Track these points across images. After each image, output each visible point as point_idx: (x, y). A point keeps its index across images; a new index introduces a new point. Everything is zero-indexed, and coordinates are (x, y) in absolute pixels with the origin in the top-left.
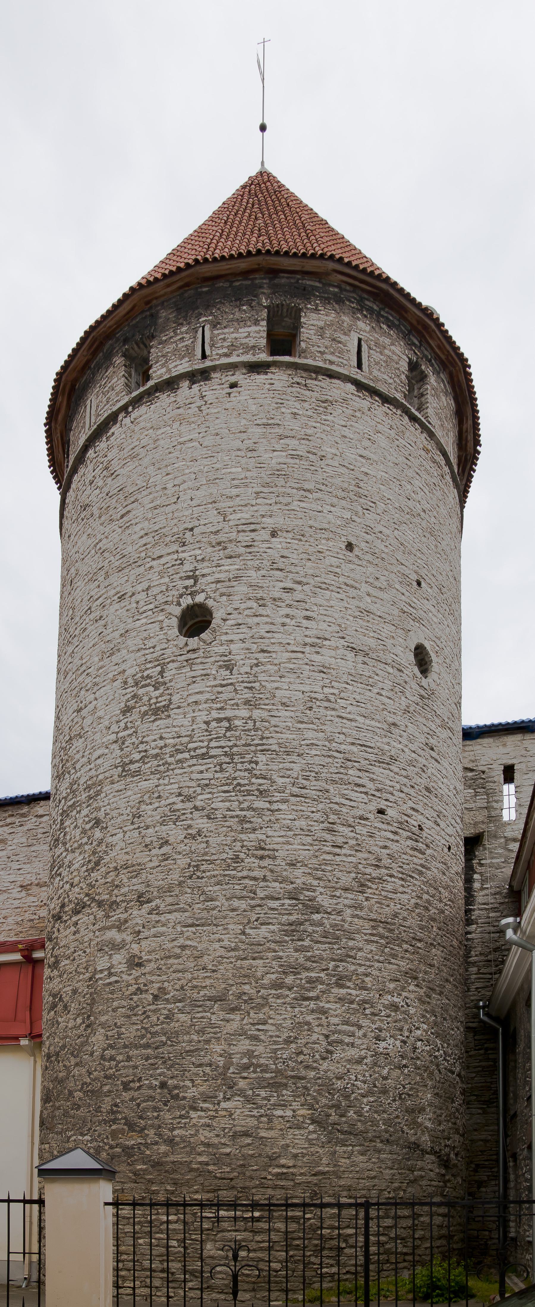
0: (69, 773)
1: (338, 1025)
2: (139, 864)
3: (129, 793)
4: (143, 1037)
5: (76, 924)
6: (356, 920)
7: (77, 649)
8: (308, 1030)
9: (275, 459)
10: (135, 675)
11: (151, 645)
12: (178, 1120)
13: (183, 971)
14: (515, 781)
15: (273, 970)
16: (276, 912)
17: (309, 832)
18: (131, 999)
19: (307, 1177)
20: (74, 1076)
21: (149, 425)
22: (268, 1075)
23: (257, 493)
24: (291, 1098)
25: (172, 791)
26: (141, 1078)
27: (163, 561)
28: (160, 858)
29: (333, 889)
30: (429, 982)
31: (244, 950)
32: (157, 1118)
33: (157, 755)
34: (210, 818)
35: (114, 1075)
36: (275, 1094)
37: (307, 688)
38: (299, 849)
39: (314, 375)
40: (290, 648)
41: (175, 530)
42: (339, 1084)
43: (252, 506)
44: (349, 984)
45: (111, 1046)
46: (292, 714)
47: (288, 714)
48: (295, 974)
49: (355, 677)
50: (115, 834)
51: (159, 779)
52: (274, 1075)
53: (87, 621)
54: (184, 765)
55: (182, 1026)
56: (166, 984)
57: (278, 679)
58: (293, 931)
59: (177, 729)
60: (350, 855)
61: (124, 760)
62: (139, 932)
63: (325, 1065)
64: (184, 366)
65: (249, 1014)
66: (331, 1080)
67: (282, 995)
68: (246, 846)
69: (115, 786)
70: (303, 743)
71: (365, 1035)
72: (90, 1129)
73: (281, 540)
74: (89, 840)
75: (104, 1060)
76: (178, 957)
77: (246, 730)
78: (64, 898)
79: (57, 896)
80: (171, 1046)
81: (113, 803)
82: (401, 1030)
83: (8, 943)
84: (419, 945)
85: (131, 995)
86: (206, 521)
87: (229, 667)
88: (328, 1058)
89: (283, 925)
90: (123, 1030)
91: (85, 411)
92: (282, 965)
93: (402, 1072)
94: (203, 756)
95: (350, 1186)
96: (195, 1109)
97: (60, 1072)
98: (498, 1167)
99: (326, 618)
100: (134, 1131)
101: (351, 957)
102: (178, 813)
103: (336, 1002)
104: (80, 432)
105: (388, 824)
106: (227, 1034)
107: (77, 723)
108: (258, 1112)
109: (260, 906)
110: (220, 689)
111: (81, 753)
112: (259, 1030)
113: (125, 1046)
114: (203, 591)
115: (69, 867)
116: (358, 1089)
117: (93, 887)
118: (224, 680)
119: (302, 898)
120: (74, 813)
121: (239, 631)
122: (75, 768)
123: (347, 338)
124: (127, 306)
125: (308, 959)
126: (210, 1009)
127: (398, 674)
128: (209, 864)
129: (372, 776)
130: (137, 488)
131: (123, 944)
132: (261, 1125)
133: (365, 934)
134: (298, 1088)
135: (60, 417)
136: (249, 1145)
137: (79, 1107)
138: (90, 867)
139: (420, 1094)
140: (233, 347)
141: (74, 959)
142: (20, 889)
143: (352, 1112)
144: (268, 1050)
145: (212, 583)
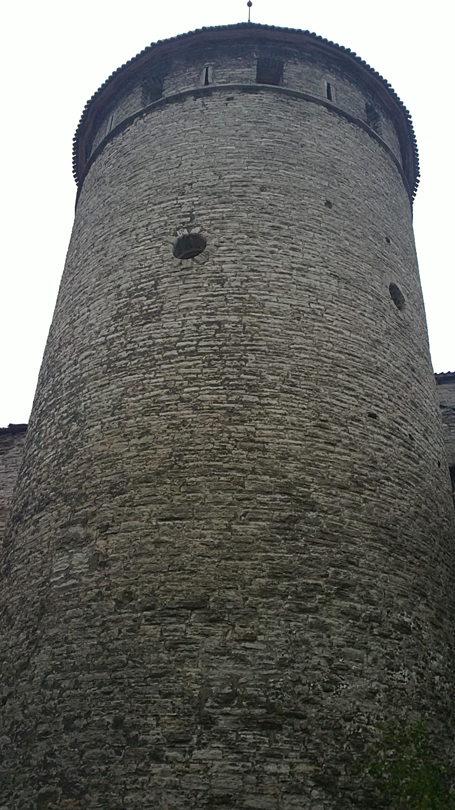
2: (116, 455)
4: (98, 655)
5: (37, 521)
6: (355, 522)
10: (129, 288)
11: (146, 265)
16: (266, 507)
17: (300, 427)
18: (89, 606)
22: (257, 711)
24: (287, 746)
26: (90, 712)
27: (163, 205)
28: (139, 448)
30: (438, 603)
31: (229, 548)
32: (104, 774)
33: (143, 354)
36: (267, 740)
37: (295, 302)
38: (291, 444)
40: (278, 270)
41: (177, 184)
44: (352, 596)
45: (56, 668)
46: (281, 322)
47: (276, 321)
48: (290, 579)
49: (339, 298)
50: (93, 426)
51: (144, 374)
54: (172, 361)
55: (149, 641)
56: (133, 588)
57: (268, 293)
58: (286, 529)
59: (167, 330)
63: (328, 700)
65: (234, 626)
68: (234, 437)
70: (291, 346)
71: (375, 661)
73: (269, 193)
74: (64, 434)
76: (150, 554)
77: (235, 333)
78: (29, 496)
80: (133, 668)
81: (94, 397)
84: (423, 558)
85: (89, 601)
87: (221, 282)
88: (332, 691)
89: (274, 522)
90: (74, 646)
91: (107, 124)
92: (274, 568)
93: (423, 715)
94: (192, 353)
99: (310, 251)
100: (70, 796)
102: (162, 405)
103: (339, 617)
105: (380, 428)
106: (206, 652)
107: (69, 332)
108: (243, 766)
109: (248, 499)
110: (211, 299)
111: (68, 357)
112: (246, 649)
113: (75, 669)
114: (199, 226)
116: (373, 736)
118: (215, 291)
119: (295, 494)
125: (304, 562)
127: (378, 302)
128: (193, 454)
129: (360, 382)
132: (248, 787)
133: (367, 539)
141: (29, 562)
144: (256, 676)
145: (207, 220)
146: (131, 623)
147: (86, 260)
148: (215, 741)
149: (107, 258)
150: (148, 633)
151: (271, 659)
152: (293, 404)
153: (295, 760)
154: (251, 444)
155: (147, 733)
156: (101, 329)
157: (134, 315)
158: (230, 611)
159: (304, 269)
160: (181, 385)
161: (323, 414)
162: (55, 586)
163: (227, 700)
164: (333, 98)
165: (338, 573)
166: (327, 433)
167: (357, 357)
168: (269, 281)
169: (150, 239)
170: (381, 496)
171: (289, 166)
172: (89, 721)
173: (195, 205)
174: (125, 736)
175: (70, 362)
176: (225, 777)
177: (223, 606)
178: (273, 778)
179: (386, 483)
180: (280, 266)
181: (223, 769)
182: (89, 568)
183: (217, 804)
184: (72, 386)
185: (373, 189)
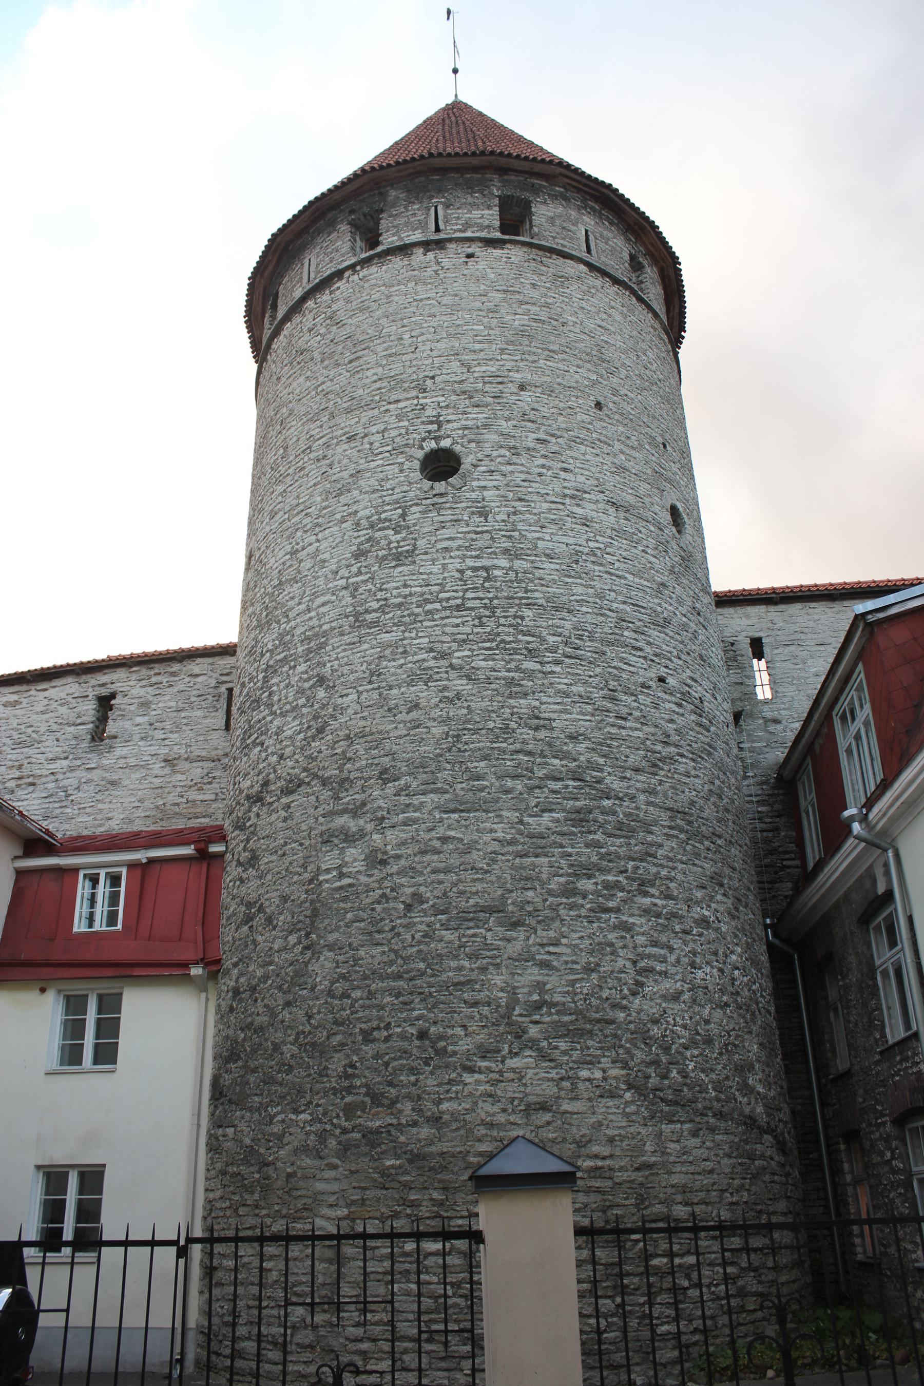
0: (278, 622)
1: (646, 947)
2: (380, 732)
3: (365, 646)
4: (391, 963)
5: (288, 806)
6: (652, 809)
7: (290, 489)
8: (612, 954)
9: (519, 321)
11: (389, 487)
12: (447, 1087)
13: (446, 871)
14: (765, 655)
15: (561, 872)
17: (587, 699)
19: (629, 1173)
20: (283, 1021)
22: (566, 1018)
24: (599, 1052)
25: (422, 646)
26: (389, 1023)
27: (401, 405)
31: (523, 844)
33: (399, 606)
34: (470, 679)
35: (348, 1019)
36: (578, 1047)
39: (548, 255)
40: (549, 498)
41: (415, 377)
42: (655, 1031)
43: (498, 360)
46: (558, 567)
47: (553, 566)
49: (619, 533)
50: (347, 695)
51: (404, 632)
52: (574, 1017)
53: (306, 459)
54: (435, 617)
56: (422, 889)
57: (539, 529)
58: (582, 820)
59: (425, 577)
60: (636, 729)
61: (358, 608)
62: (383, 818)
64: (417, 236)
66: (645, 1024)
67: (576, 906)
69: (346, 637)
71: (678, 961)
72: (310, 1102)
73: (530, 393)
74: (308, 701)
75: (333, 997)
79: (256, 771)
80: (432, 976)
81: (343, 658)
82: (715, 954)
83: (143, 835)
84: (719, 842)
85: (373, 903)
86: (449, 371)
87: (484, 514)
92: (572, 865)
93: (724, 1013)
94: (458, 608)
95: (684, 1186)
96: (471, 1070)
97: (258, 1015)
98: (819, 1150)
99: (583, 471)
101: (651, 855)
103: (641, 916)
104: (295, 286)
105: (671, 694)
107: (291, 566)
110: (474, 536)
111: (296, 600)
112: (549, 953)
113: (365, 977)
114: (449, 436)
115: (277, 734)
117: (314, 759)
118: (478, 527)
119: (588, 779)
120: (286, 669)
121: (491, 478)
123: (575, 228)
124: (356, 184)
125: (602, 857)
126: (485, 924)
127: (660, 533)
129: (648, 638)
130: (368, 337)
131: (362, 834)
132: (563, 1093)
134: (606, 1037)
135: (267, 274)
136: (549, 1123)
137: (290, 1069)
138: (309, 734)
139: (746, 1045)
140: (467, 226)
141: (284, 854)
142: (163, 764)
143: (675, 1071)
144: (563, 982)
145: (459, 429)
147: (303, 468)
148: (526, 1050)
150: (445, 939)
151: (577, 963)
152: (579, 672)
153: (608, 1066)
154: (536, 721)
155: (455, 1044)
156: (339, 568)
157: (380, 553)
158: (529, 914)
159: (578, 496)
160: (450, 648)
161: (611, 682)
163: (537, 1007)
164: (593, 252)
167: (644, 608)
168: (539, 514)
170: (676, 776)
171: (551, 354)
172: (391, 1032)
173: (441, 407)
174: (432, 1047)
175: (301, 607)
176: (540, 1085)
177: (522, 908)
178: (587, 1083)
179: (680, 760)
180: (551, 493)
181: (537, 1077)
182: (367, 866)
183: (534, 1110)
184: (309, 639)
185: (646, 378)
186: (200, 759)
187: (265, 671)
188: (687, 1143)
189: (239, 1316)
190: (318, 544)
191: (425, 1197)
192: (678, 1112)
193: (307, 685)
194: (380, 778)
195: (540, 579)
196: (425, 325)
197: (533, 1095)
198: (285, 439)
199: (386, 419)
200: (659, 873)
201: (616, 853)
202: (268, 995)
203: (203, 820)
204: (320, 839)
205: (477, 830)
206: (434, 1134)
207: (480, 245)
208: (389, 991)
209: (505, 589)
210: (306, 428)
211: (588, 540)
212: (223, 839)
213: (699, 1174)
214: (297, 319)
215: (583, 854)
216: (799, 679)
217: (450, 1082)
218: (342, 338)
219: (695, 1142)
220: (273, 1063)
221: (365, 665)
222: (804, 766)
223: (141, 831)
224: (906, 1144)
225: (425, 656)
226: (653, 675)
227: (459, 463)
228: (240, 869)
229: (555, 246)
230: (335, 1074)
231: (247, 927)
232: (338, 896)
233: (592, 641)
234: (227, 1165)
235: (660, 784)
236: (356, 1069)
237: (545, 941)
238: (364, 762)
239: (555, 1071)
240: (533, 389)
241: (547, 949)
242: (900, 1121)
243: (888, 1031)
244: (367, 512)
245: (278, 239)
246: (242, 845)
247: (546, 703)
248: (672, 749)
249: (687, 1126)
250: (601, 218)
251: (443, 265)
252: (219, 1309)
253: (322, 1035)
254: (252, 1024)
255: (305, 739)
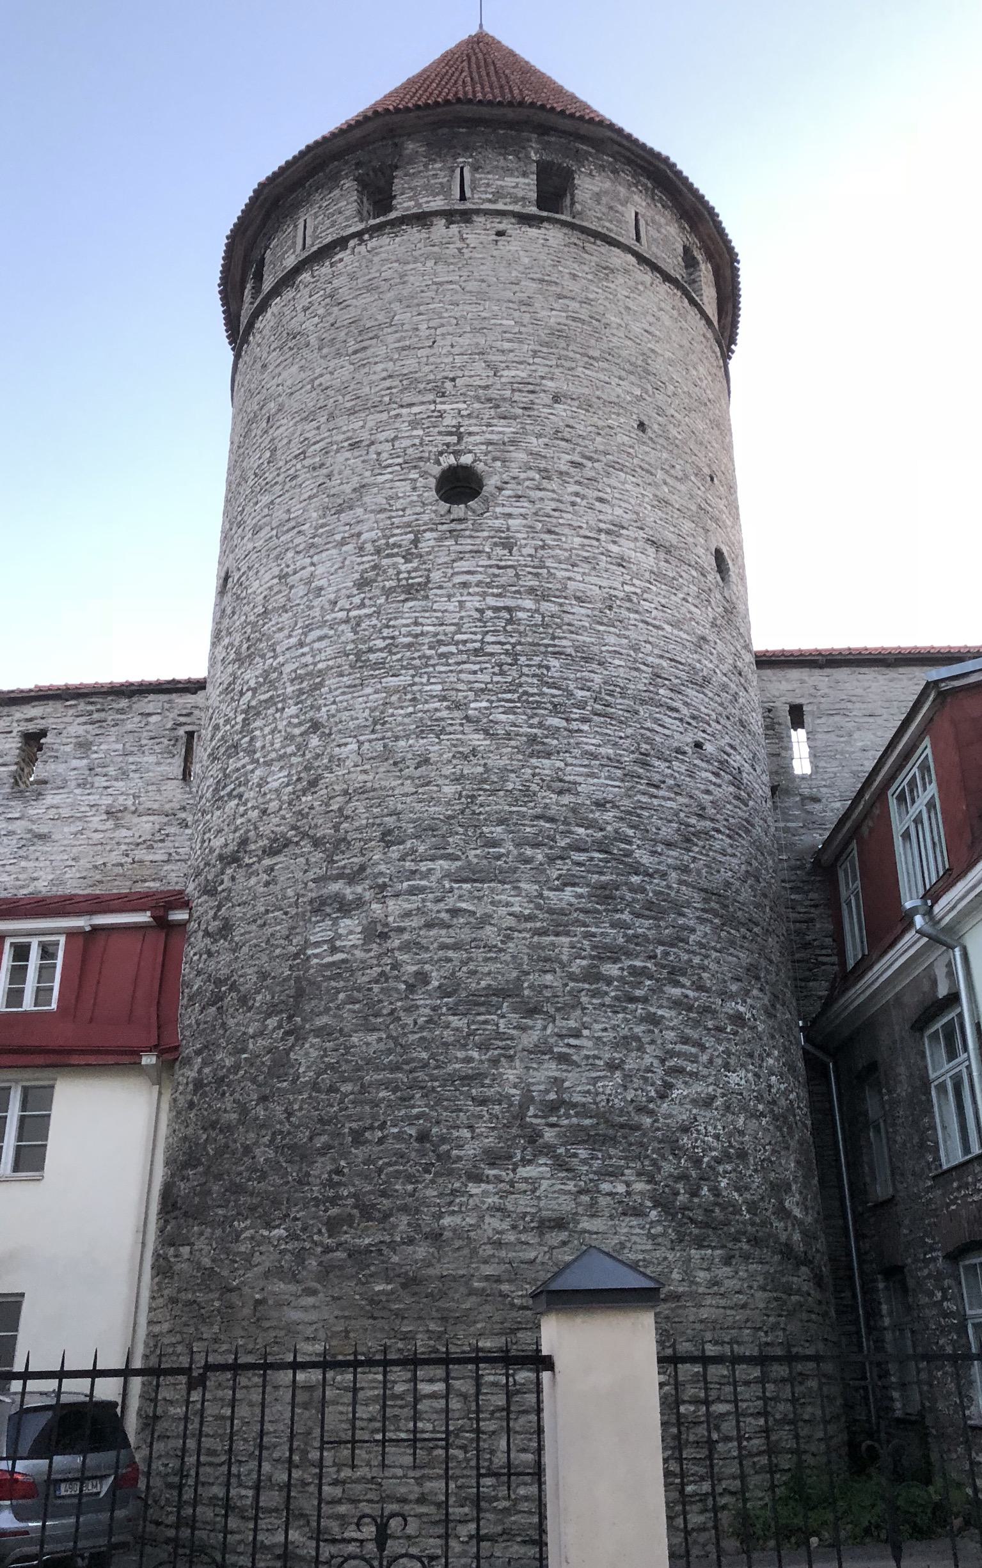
0: (263, 656)
3: (368, 690)
4: (389, 1052)
5: (271, 869)
6: (684, 888)
7: (279, 500)
8: (638, 1050)
9: (555, 318)
11: (399, 507)
12: (448, 1199)
13: (456, 947)
15: (584, 953)
21: (394, 258)
22: (587, 1122)
23: (535, 352)
26: (385, 1122)
27: (415, 410)
29: (653, 842)
31: (542, 920)
33: (409, 646)
37: (605, 583)
39: (592, 240)
40: (582, 532)
41: (432, 377)
46: (589, 612)
47: (583, 611)
49: (658, 576)
50: (346, 744)
51: (413, 676)
53: (299, 466)
54: (450, 661)
58: (607, 897)
59: (439, 614)
60: (669, 799)
64: (438, 203)
69: (345, 679)
71: (711, 1061)
73: (566, 407)
74: (298, 750)
75: (319, 1091)
79: (233, 827)
80: (436, 1067)
81: (341, 702)
84: (756, 930)
85: (369, 982)
86: (472, 373)
87: (508, 545)
94: (477, 653)
96: (478, 1178)
97: (225, 1111)
100: (370, 1219)
101: (682, 940)
103: (670, 1008)
104: (286, 252)
105: (708, 762)
110: (496, 571)
111: (286, 632)
112: (569, 1045)
114: (470, 452)
115: (260, 786)
118: (501, 560)
119: (615, 851)
120: (271, 711)
121: (518, 504)
122: (274, 650)
125: (629, 939)
127: (703, 579)
131: (359, 903)
132: (580, 1210)
134: (631, 1145)
137: (263, 1177)
138: (299, 787)
141: (265, 924)
142: (105, 817)
143: (706, 1188)
145: (482, 444)
146: (427, 1011)
147: (295, 477)
149: (333, 483)
150: (453, 1025)
151: (600, 1058)
152: (608, 731)
154: (561, 784)
155: (460, 1147)
159: (615, 531)
160: (465, 697)
161: (644, 746)
162: (315, 961)
165: (667, 954)
166: (648, 771)
169: (400, 464)
170: (711, 853)
174: (433, 1151)
177: (540, 992)
178: (609, 1198)
180: (585, 526)
183: (549, 1227)
184: (301, 679)
186: (150, 812)
187: (246, 712)
188: (717, 1272)
189: (187, 1476)
190: (313, 568)
191: (421, 1329)
192: (709, 1236)
193: (297, 731)
194: (382, 840)
195: (569, 624)
196: (445, 315)
197: (548, 1210)
198: (273, 439)
199: (397, 425)
200: (691, 961)
201: (645, 935)
202: (238, 1089)
203: (151, 884)
204: (309, 908)
205: (491, 903)
206: (433, 1254)
207: (513, 220)
208: (385, 1084)
209: (530, 633)
210: (300, 427)
211: (623, 583)
212: (186, 905)
213: (732, 1308)
214: (289, 294)
215: (608, 934)
216: (842, 753)
217: (454, 1192)
218: (345, 323)
219: (727, 1270)
220: (243, 1168)
221: (367, 711)
222: (849, 850)
223: (75, 895)
224: (960, 1283)
225: (437, 705)
226: (689, 740)
227: (481, 486)
228: (208, 941)
229: (600, 229)
230: (318, 1181)
231: (214, 1009)
232: (329, 973)
233: (624, 698)
234: (179, 1291)
235: (693, 862)
236: (344, 1175)
237: (564, 1032)
238: (364, 822)
239: (572, 1183)
240: (569, 401)
241: (566, 1041)
242: (955, 1256)
243: (942, 1153)
244: (372, 535)
245: (266, 191)
246: (211, 913)
247: (571, 765)
248: (708, 824)
249: (719, 1252)
250: (653, 199)
251: (468, 241)
252: (162, 1468)
253: (303, 1136)
254: (217, 1122)
255: (294, 793)
